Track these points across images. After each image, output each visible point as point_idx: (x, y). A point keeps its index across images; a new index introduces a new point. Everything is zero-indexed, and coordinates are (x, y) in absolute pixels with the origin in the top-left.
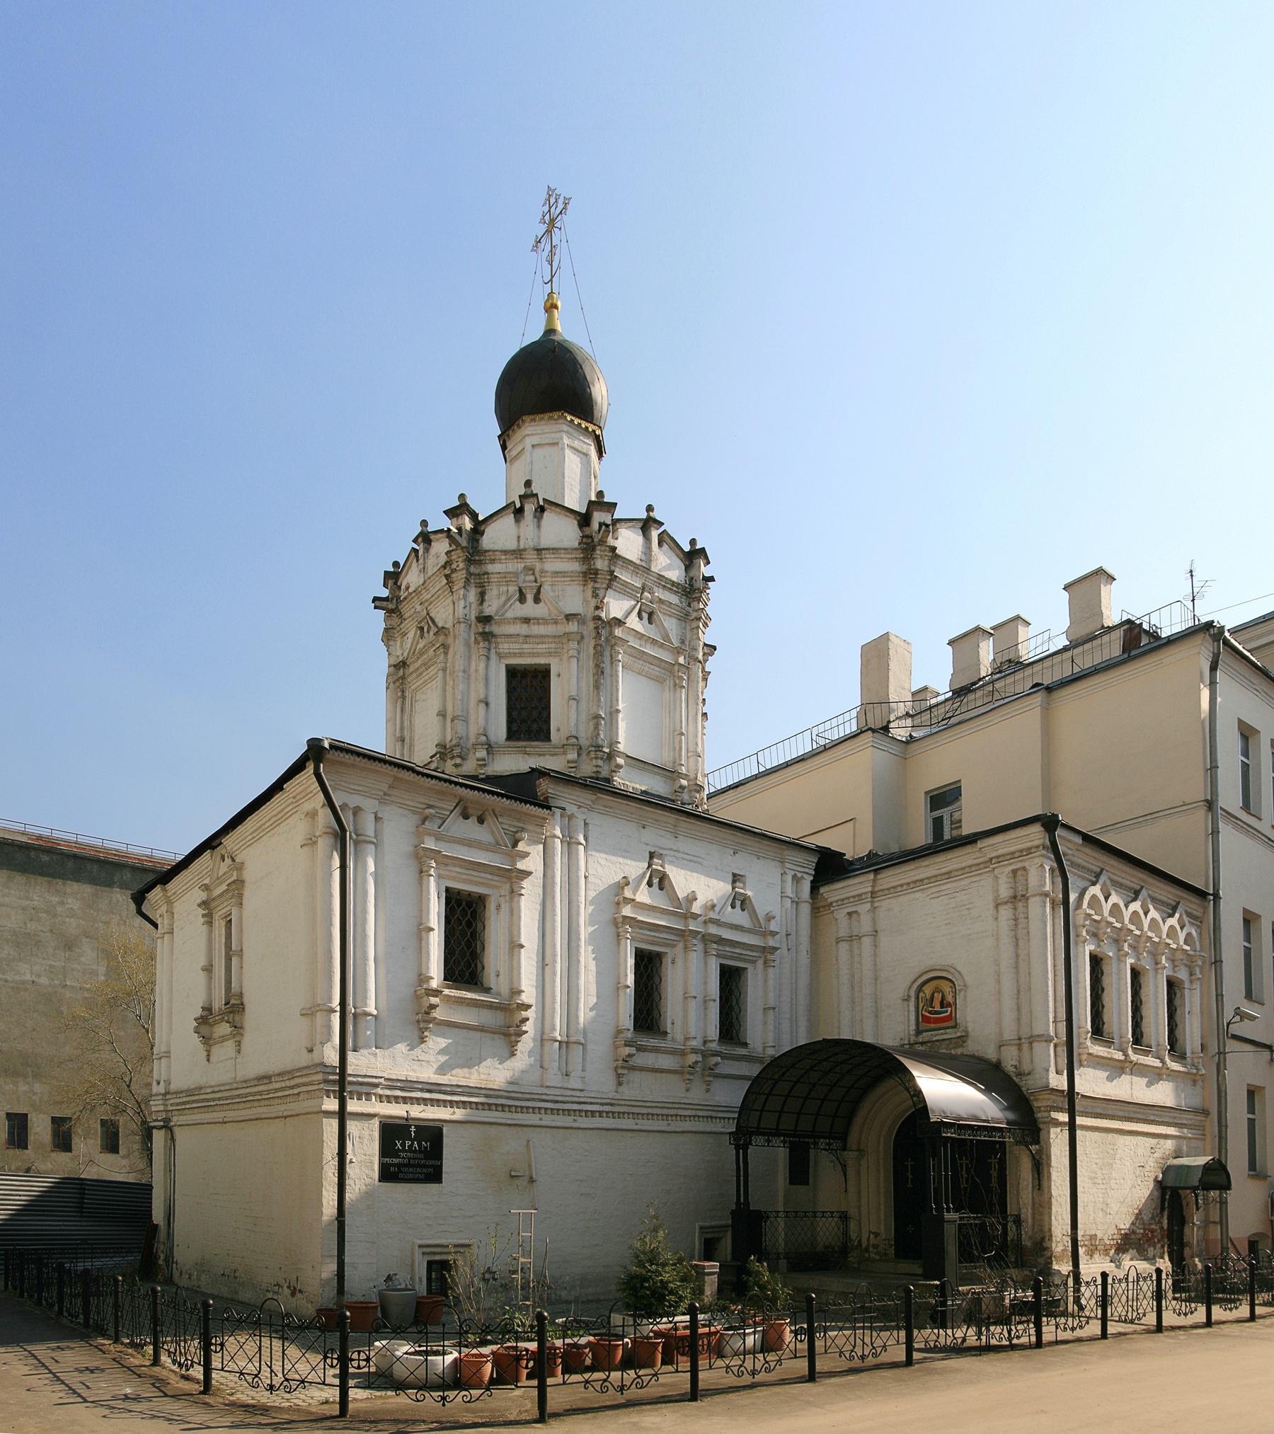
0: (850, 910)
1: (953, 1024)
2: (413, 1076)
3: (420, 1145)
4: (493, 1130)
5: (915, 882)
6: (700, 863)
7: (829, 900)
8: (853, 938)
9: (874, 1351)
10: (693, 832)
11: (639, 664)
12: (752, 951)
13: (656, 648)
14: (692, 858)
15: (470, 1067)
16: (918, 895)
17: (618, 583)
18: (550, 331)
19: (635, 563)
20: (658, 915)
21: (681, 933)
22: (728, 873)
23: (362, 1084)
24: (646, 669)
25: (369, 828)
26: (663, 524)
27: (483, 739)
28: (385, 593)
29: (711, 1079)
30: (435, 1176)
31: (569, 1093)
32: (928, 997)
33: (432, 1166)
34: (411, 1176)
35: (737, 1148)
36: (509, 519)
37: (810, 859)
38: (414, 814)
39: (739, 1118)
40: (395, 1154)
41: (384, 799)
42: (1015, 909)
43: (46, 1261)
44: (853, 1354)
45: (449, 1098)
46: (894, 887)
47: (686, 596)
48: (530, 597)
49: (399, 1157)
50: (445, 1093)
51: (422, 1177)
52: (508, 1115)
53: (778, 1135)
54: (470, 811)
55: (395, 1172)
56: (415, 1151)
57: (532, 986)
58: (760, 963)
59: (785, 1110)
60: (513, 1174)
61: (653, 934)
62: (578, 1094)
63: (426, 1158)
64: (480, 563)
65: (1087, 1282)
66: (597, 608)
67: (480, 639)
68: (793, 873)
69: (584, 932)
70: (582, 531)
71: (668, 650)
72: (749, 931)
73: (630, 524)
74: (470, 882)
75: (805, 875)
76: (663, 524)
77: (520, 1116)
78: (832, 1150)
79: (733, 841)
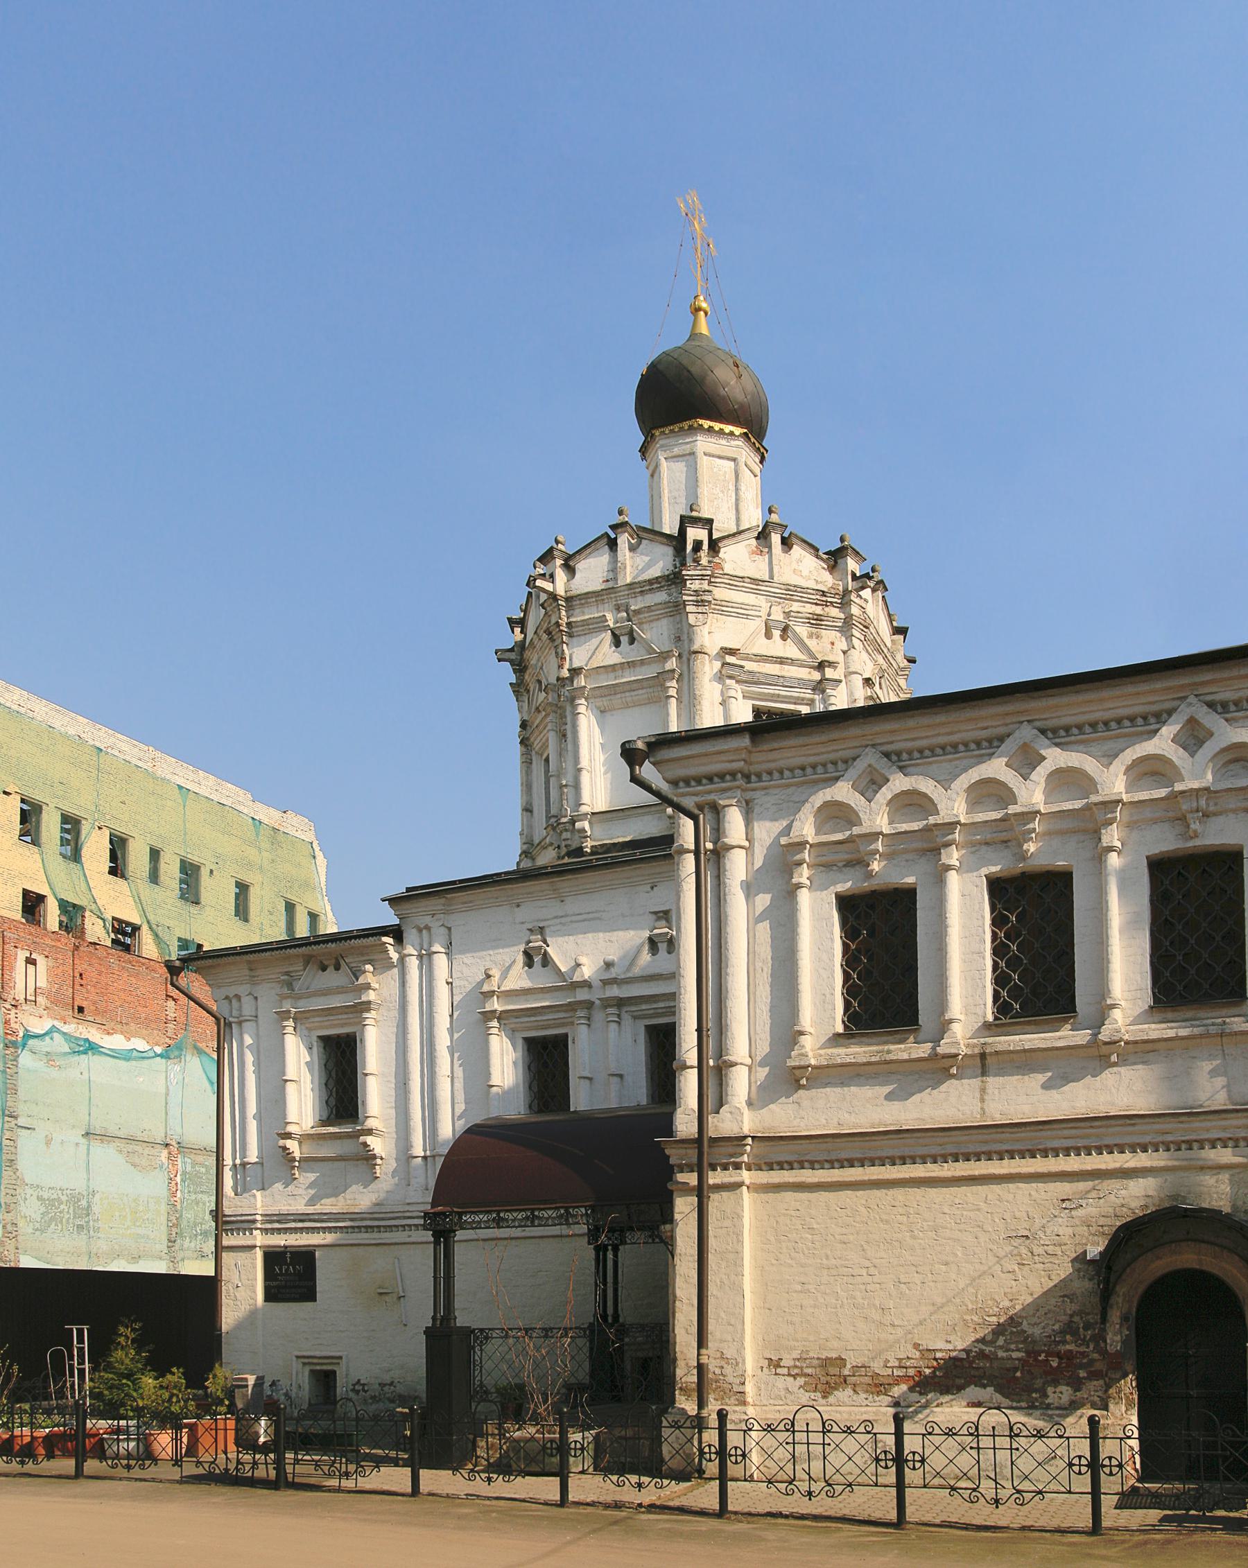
1: (811, 1049)
2: (285, 1209)
4: (360, 1250)
6: (599, 919)
10: (581, 887)
11: (617, 700)
13: (638, 669)
14: (585, 916)
15: (336, 1195)
17: (577, 627)
20: (541, 996)
21: (571, 1007)
22: (644, 914)
23: (242, 1222)
24: (629, 699)
41: (253, 981)
43: (1042, 1357)
45: (318, 1225)
47: (674, 583)
49: (277, 1280)
50: (314, 1221)
52: (376, 1235)
54: (326, 963)
57: (391, 1108)
61: (533, 1019)
69: (443, 1040)
71: (655, 662)
73: (589, 551)
74: (335, 1026)
77: (388, 1235)
79: (643, 876)
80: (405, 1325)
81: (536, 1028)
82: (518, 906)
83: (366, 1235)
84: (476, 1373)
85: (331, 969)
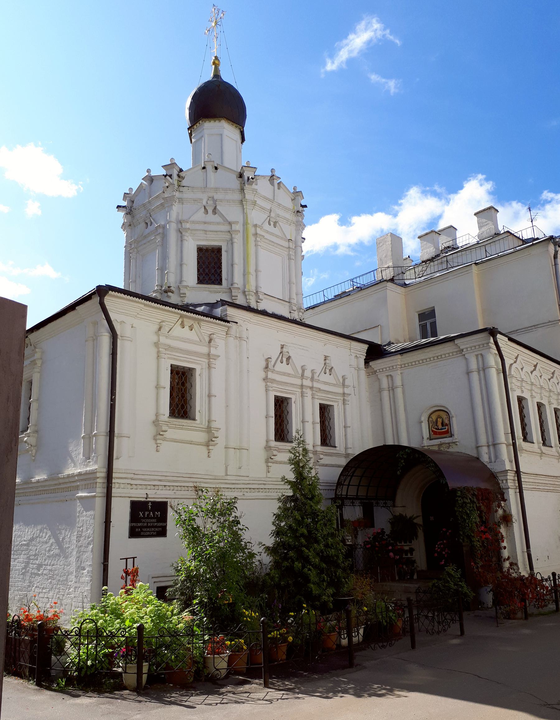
0: (388, 374)
7: (375, 369)
9: (444, 628)
28: (125, 204)
32: (434, 420)
33: (159, 527)
39: (336, 490)
44: (434, 631)
48: (210, 211)
49: (140, 522)
51: (155, 533)
59: (361, 484)
65: (546, 579)
68: (355, 355)
72: (334, 385)
78: (388, 506)
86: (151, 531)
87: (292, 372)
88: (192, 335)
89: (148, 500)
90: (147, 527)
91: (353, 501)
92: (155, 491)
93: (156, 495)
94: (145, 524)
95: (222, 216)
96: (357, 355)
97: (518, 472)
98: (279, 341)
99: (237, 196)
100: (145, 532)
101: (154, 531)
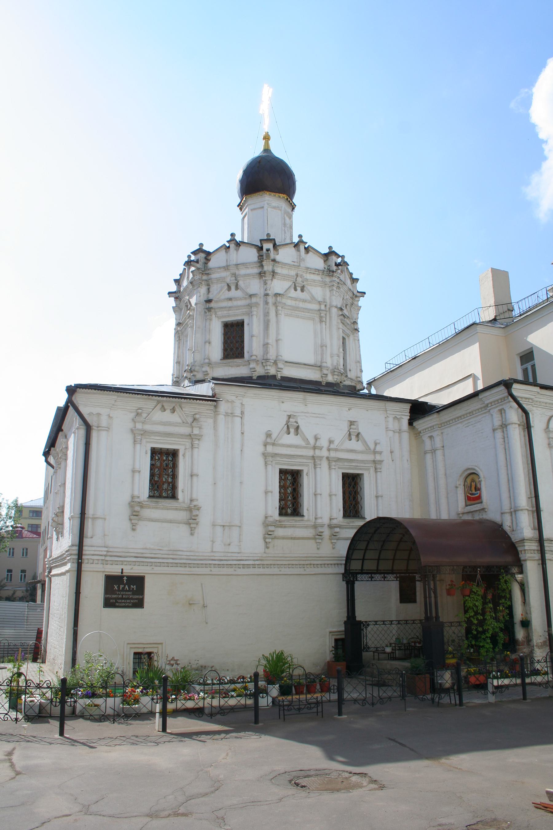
3: (129, 587)
5: (458, 418)
8: (433, 451)
12: (365, 464)
16: (460, 425)
18: (267, 150)
19: (289, 264)
25: (104, 422)
26: (307, 243)
27: (207, 361)
29: (335, 541)
30: (140, 604)
31: (230, 555)
32: (469, 485)
33: (136, 599)
34: (123, 604)
35: (347, 583)
36: (223, 252)
37: (405, 407)
38: (132, 413)
40: (114, 592)
42: (503, 432)
46: (449, 421)
48: (233, 288)
49: (116, 594)
52: (188, 569)
53: (392, 573)
54: (166, 407)
55: (113, 602)
56: (126, 591)
58: (372, 470)
60: (191, 602)
62: (236, 555)
63: (133, 594)
64: (208, 274)
66: (266, 290)
67: (206, 311)
68: (394, 416)
70: (258, 253)
72: (362, 452)
75: (403, 417)
76: (307, 243)
77: (196, 569)
80: (207, 623)
81: (288, 465)
82: (283, 402)
83: (166, 568)
84: (364, 639)
85: (168, 411)
86: (127, 603)
87: (303, 443)
88: (175, 418)
89: (124, 574)
90: (122, 599)
91: (371, 575)
92: (130, 567)
93: (131, 570)
94: (120, 596)
95: (243, 290)
96: (397, 416)
97: (541, 540)
98: (285, 411)
99: (256, 270)
100: (120, 603)
101: (130, 603)
